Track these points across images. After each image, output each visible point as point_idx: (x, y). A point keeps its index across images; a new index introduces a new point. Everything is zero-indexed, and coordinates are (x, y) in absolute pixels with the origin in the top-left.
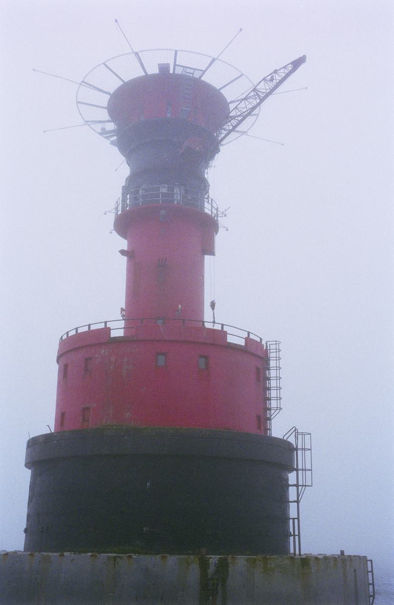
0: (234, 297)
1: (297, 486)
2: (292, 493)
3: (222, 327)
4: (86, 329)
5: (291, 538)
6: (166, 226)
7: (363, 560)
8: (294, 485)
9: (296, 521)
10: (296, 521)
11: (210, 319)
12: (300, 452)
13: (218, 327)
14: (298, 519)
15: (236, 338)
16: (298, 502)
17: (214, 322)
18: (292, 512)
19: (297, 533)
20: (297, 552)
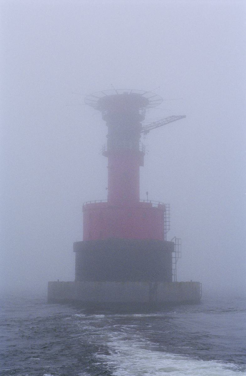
0: (152, 188)
1: (176, 258)
2: (174, 260)
3: (150, 201)
4: (100, 202)
5: (173, 276)
6: (125, 158)
7: (198, 283)
8: (174, 258)
9: (175, 270)
10: (175, 276)
11: (143, 198)
12: (177, 246)
13: (149, 202)
14: (176, 269)
15: (155, 205)
16: (176, 263)
17: (148, 200)
18: (174, 267)
19: (175, 274)
20: (175, 281)
